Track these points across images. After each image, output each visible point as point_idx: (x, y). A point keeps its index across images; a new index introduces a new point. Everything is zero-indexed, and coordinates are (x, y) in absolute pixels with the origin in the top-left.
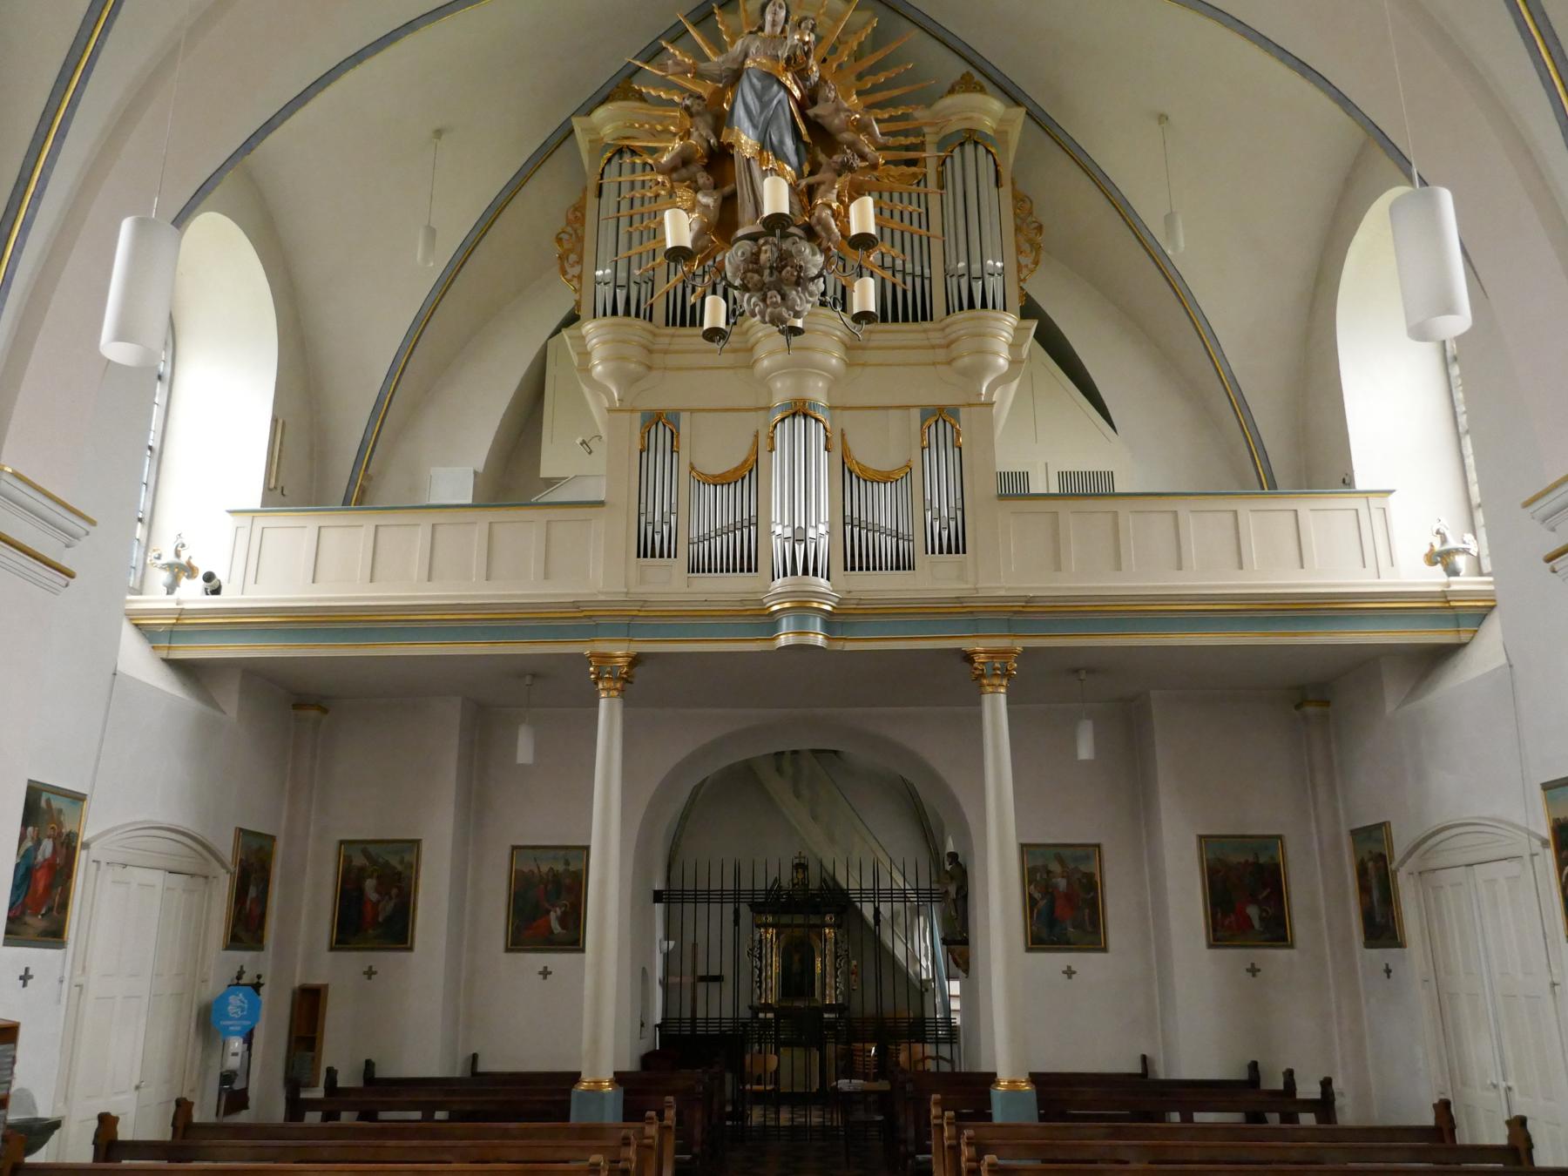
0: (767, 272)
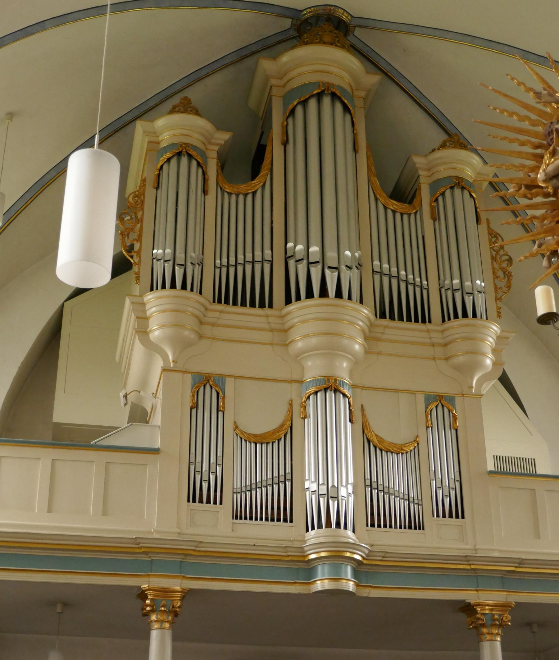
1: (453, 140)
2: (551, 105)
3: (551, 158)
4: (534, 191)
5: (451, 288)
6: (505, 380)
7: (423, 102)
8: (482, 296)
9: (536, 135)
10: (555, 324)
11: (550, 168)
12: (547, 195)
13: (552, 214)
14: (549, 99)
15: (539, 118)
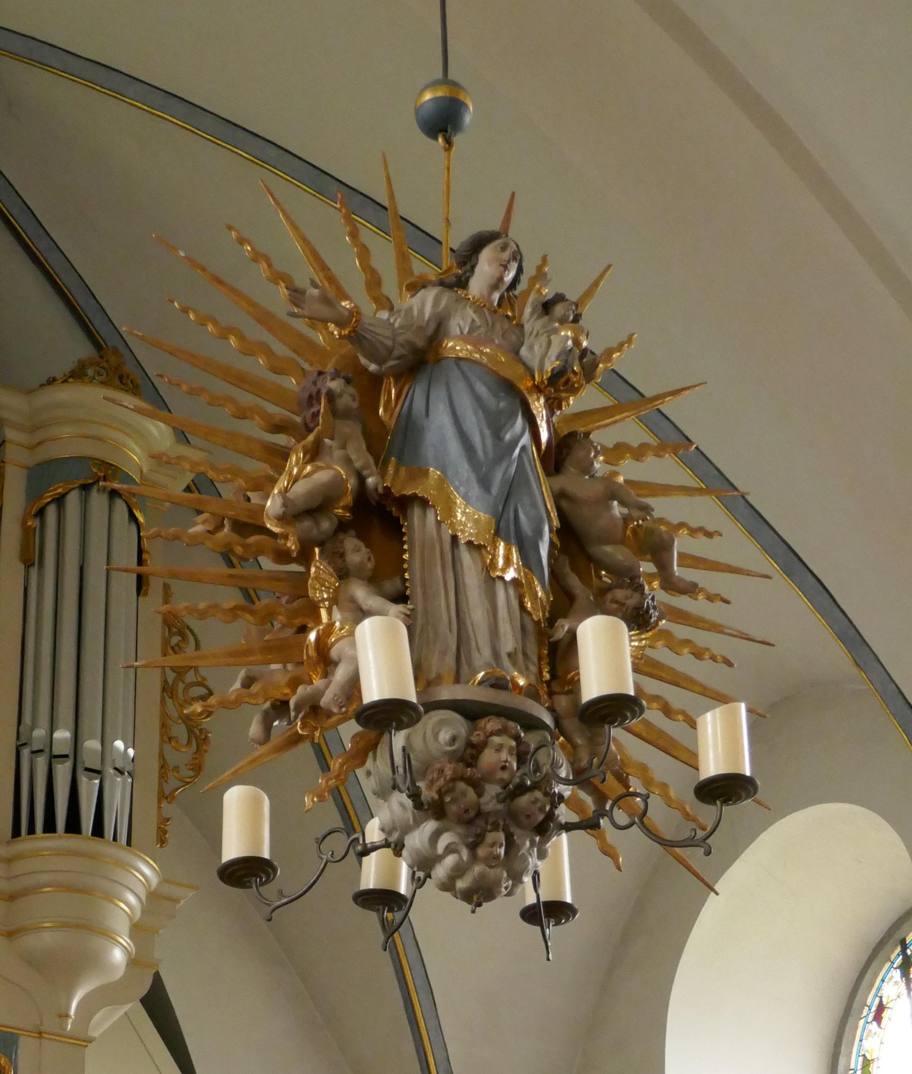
0: (492, 790)
1: (105, 365)
2: (327, 328)
3: (307, 463)
4: (252, 539)
5: (47, 750)
6: (157, 1006)
7: (41, 246)
8: (124, 783)
9: (279, 396)
10: (260, 889)
11: (300, 489)
12: (283, 556)
13: (289, 606)
14: (323, 310)
15: (294, 356)
